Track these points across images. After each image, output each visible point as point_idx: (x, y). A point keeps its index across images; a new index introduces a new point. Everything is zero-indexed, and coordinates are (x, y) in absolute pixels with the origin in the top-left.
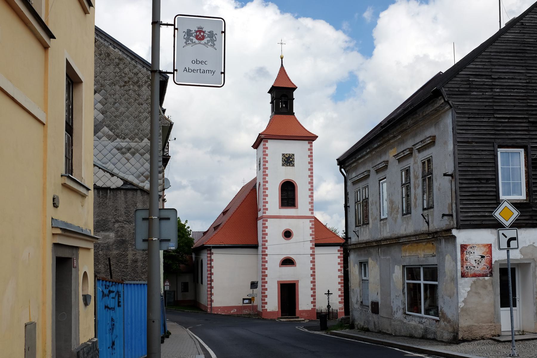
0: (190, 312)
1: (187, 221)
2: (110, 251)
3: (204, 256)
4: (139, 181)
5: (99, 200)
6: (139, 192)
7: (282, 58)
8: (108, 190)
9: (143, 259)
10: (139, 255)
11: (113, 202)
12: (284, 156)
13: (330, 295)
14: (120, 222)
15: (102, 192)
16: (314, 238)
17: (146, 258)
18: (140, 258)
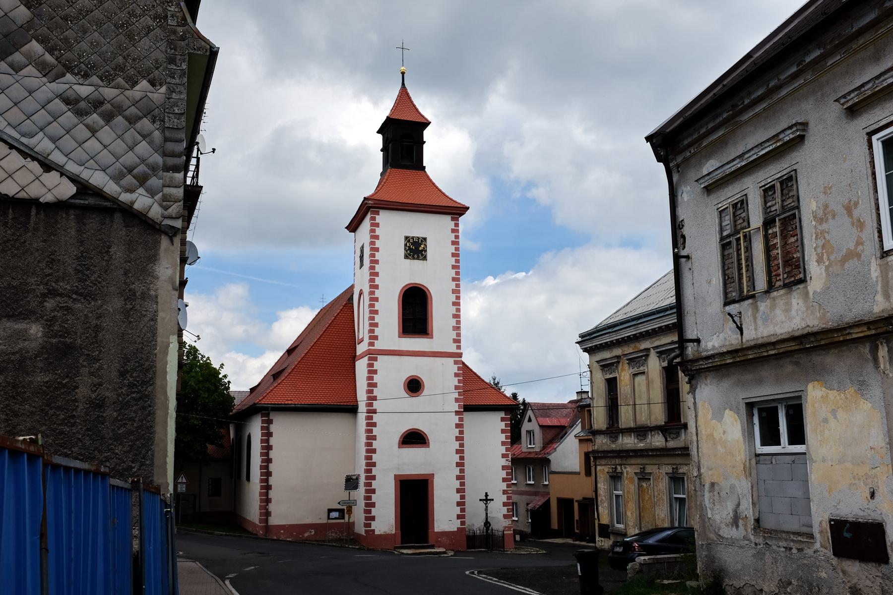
0: (226, 535)
1: (223, 364)
2: (28, 374)
3: (255, 429)
4: (120, 187)
5: (6, 231)
6: (118, 217)
7: (403, 73)
8: (31, 209)
9: (121, 399)
10: (108, 389)
11: (45, 241)
12: (409, 241)
13: (488, 502)
14: (61, 295)
15: (13, 211)
16: (462, 393)
17: (128, 395)
18: (110, 395)
